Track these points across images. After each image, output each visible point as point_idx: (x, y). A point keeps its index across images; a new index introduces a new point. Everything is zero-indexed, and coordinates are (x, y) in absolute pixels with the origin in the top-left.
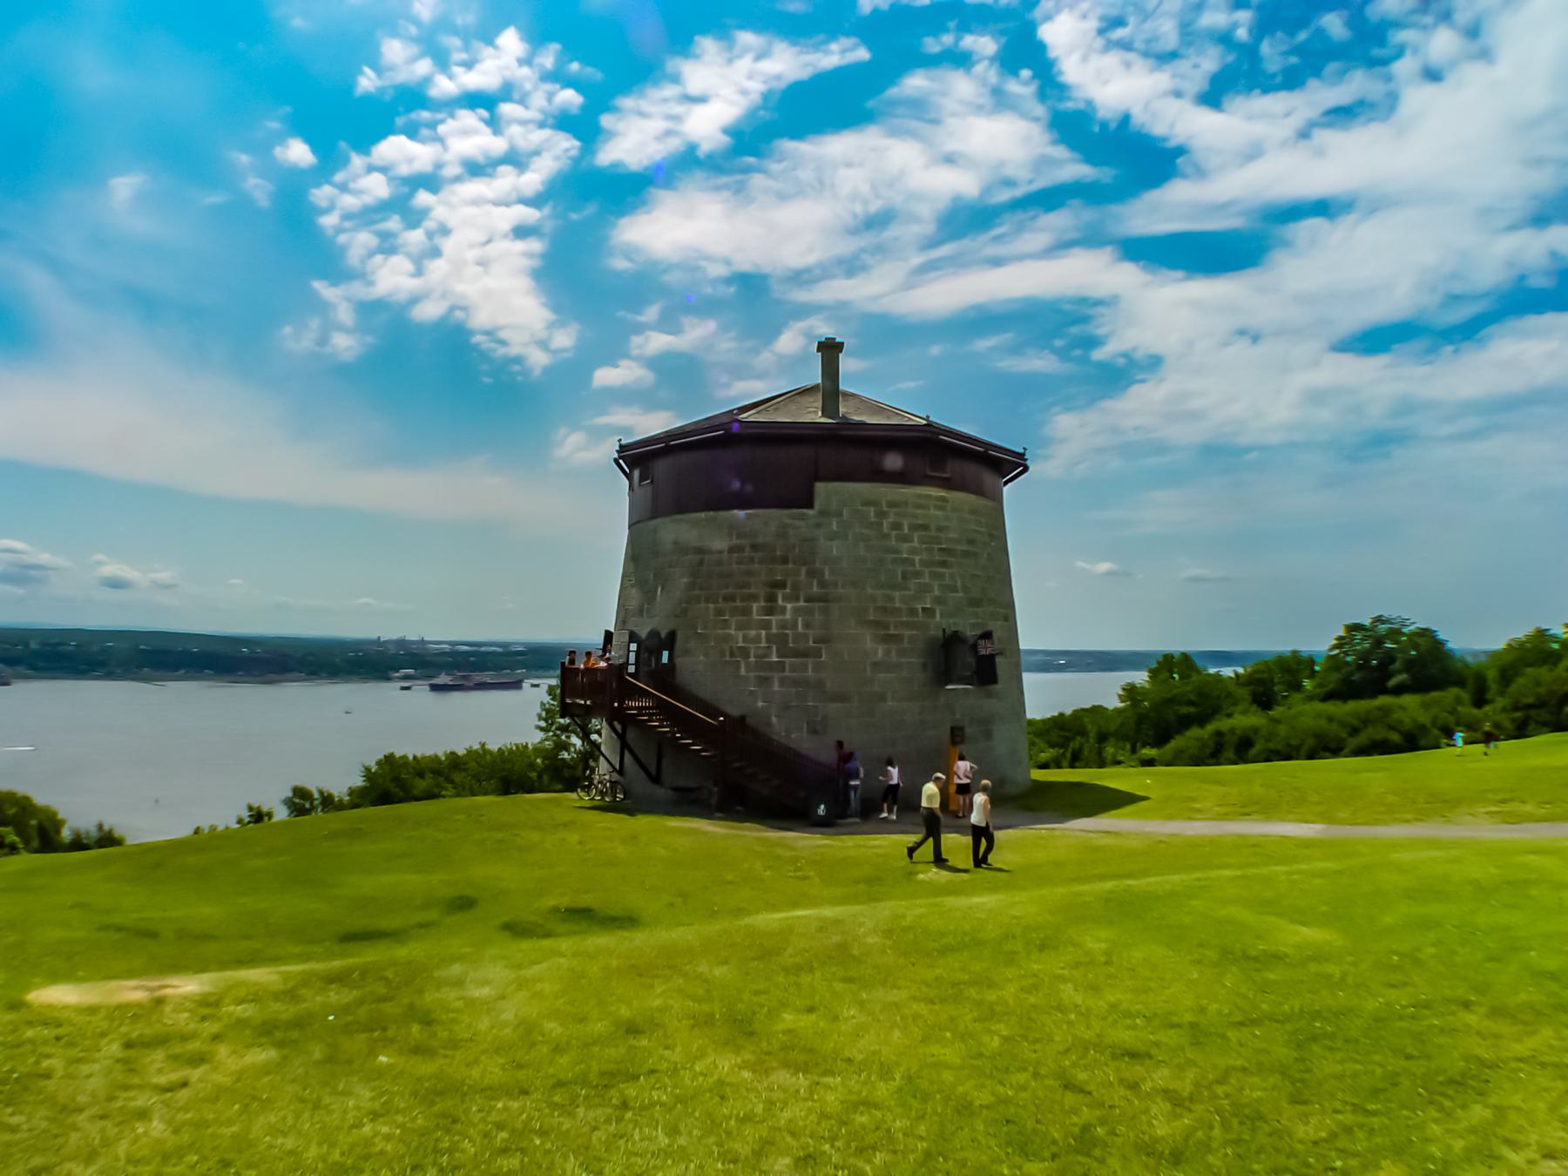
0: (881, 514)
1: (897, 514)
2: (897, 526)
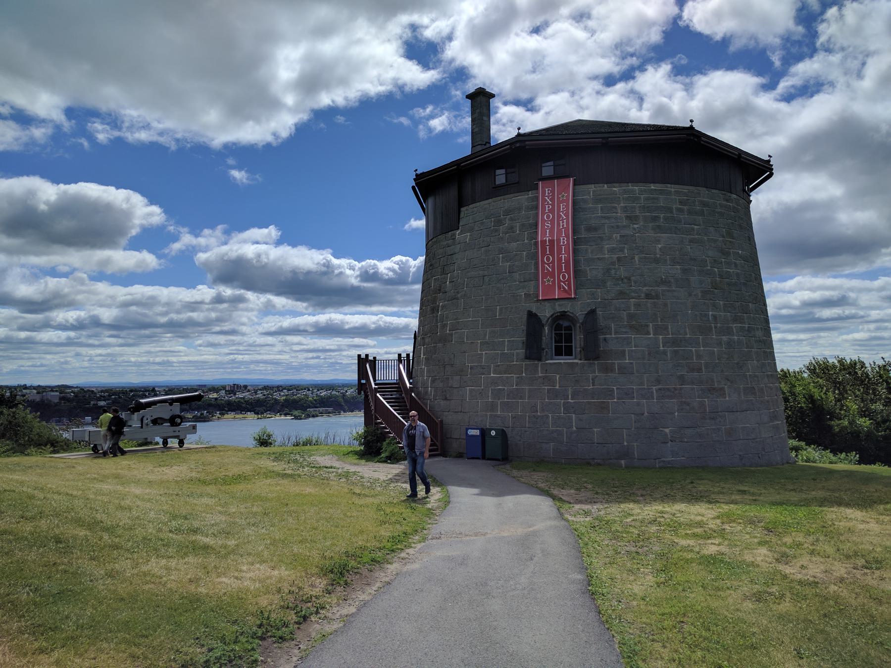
0: (499, 222)
1: (511, 219)
2: (511, 228)
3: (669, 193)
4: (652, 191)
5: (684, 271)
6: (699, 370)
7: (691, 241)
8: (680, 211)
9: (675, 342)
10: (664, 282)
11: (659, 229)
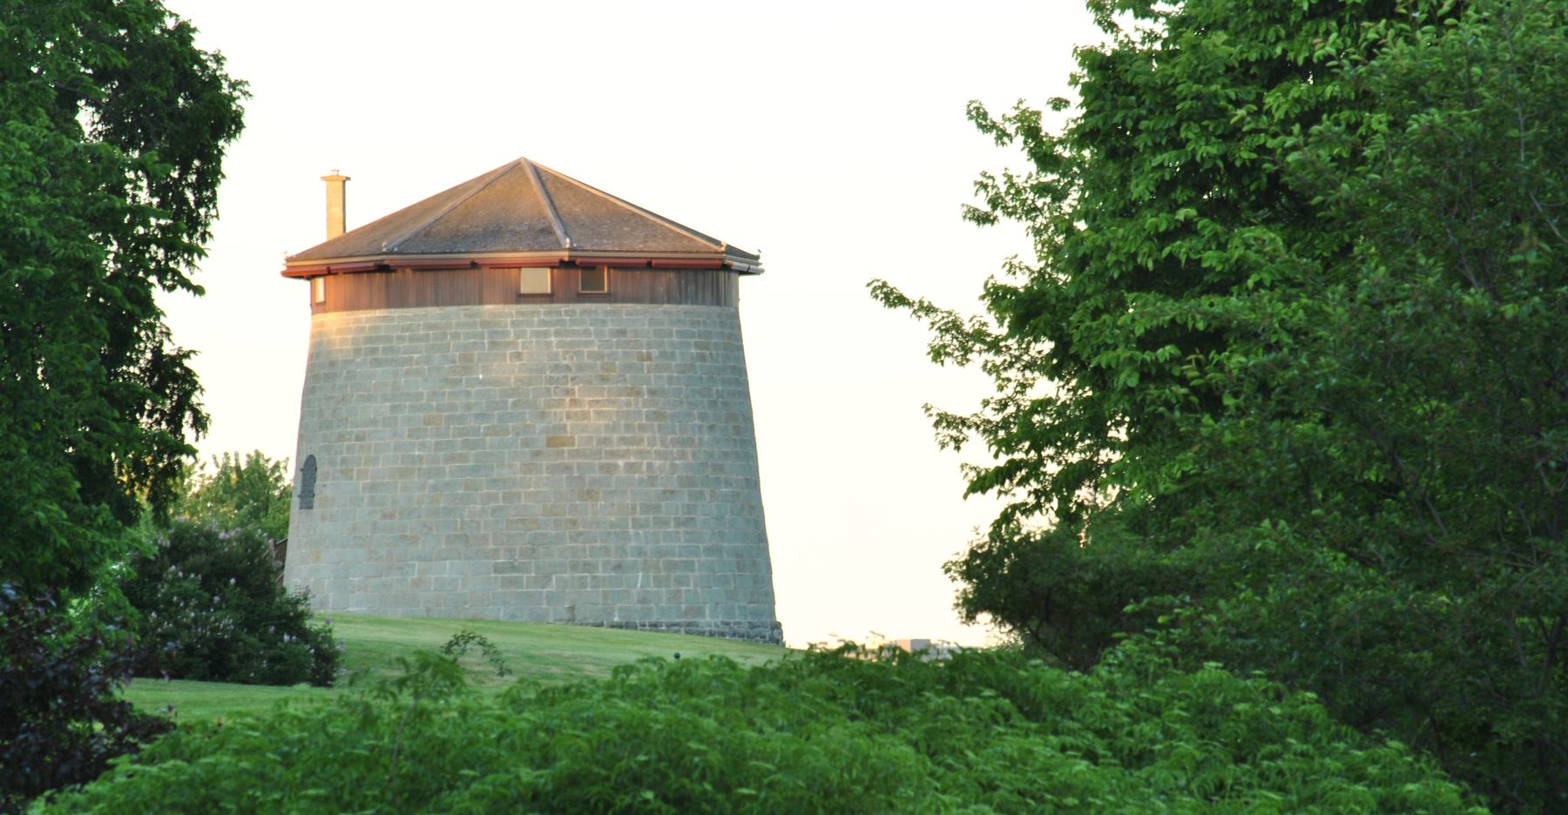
3: (392, 319)
4: (523, 314)
5: (394, 408)
6: (392, 516)
7: (408, 373)
8: (400, 338)
9: (373, 487)
10: (374, 422)
11: (377, 363)
